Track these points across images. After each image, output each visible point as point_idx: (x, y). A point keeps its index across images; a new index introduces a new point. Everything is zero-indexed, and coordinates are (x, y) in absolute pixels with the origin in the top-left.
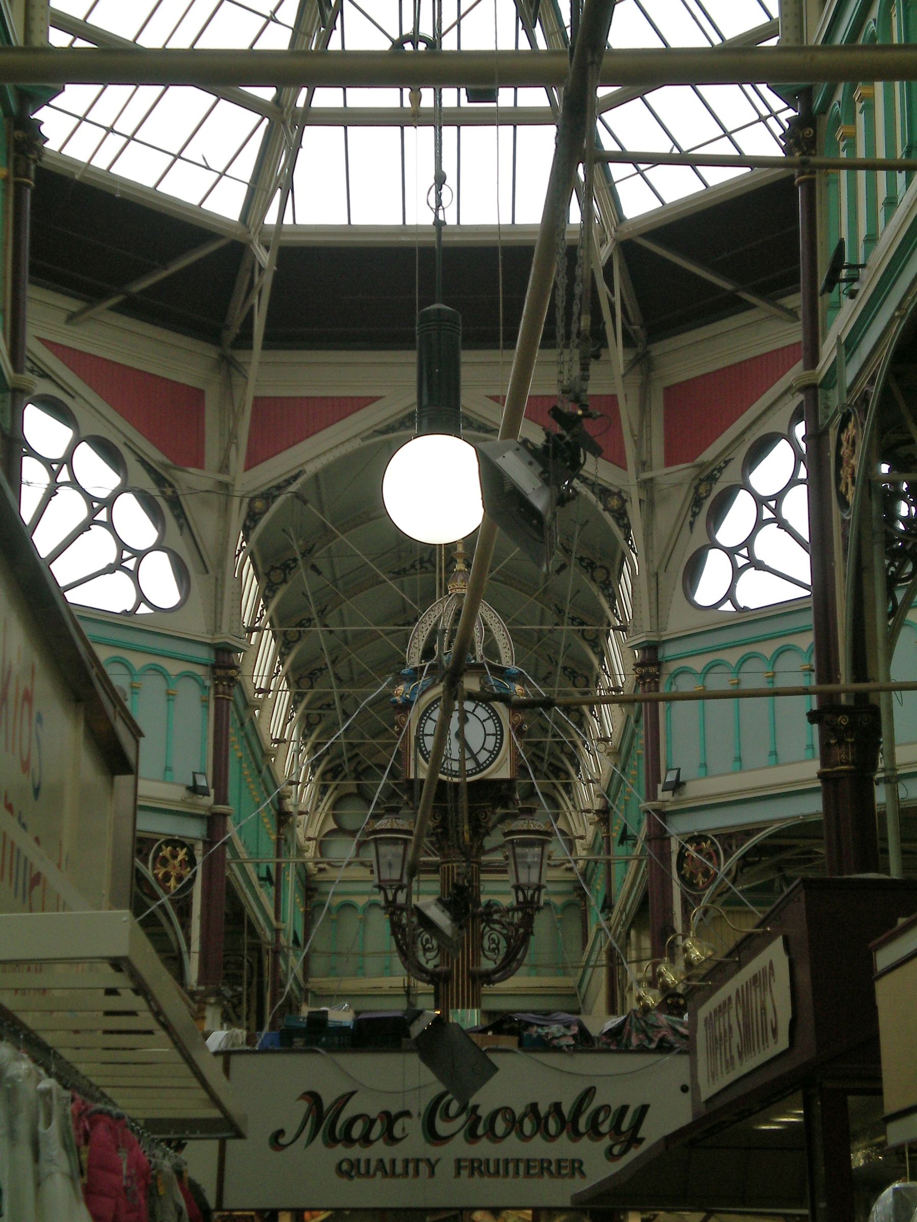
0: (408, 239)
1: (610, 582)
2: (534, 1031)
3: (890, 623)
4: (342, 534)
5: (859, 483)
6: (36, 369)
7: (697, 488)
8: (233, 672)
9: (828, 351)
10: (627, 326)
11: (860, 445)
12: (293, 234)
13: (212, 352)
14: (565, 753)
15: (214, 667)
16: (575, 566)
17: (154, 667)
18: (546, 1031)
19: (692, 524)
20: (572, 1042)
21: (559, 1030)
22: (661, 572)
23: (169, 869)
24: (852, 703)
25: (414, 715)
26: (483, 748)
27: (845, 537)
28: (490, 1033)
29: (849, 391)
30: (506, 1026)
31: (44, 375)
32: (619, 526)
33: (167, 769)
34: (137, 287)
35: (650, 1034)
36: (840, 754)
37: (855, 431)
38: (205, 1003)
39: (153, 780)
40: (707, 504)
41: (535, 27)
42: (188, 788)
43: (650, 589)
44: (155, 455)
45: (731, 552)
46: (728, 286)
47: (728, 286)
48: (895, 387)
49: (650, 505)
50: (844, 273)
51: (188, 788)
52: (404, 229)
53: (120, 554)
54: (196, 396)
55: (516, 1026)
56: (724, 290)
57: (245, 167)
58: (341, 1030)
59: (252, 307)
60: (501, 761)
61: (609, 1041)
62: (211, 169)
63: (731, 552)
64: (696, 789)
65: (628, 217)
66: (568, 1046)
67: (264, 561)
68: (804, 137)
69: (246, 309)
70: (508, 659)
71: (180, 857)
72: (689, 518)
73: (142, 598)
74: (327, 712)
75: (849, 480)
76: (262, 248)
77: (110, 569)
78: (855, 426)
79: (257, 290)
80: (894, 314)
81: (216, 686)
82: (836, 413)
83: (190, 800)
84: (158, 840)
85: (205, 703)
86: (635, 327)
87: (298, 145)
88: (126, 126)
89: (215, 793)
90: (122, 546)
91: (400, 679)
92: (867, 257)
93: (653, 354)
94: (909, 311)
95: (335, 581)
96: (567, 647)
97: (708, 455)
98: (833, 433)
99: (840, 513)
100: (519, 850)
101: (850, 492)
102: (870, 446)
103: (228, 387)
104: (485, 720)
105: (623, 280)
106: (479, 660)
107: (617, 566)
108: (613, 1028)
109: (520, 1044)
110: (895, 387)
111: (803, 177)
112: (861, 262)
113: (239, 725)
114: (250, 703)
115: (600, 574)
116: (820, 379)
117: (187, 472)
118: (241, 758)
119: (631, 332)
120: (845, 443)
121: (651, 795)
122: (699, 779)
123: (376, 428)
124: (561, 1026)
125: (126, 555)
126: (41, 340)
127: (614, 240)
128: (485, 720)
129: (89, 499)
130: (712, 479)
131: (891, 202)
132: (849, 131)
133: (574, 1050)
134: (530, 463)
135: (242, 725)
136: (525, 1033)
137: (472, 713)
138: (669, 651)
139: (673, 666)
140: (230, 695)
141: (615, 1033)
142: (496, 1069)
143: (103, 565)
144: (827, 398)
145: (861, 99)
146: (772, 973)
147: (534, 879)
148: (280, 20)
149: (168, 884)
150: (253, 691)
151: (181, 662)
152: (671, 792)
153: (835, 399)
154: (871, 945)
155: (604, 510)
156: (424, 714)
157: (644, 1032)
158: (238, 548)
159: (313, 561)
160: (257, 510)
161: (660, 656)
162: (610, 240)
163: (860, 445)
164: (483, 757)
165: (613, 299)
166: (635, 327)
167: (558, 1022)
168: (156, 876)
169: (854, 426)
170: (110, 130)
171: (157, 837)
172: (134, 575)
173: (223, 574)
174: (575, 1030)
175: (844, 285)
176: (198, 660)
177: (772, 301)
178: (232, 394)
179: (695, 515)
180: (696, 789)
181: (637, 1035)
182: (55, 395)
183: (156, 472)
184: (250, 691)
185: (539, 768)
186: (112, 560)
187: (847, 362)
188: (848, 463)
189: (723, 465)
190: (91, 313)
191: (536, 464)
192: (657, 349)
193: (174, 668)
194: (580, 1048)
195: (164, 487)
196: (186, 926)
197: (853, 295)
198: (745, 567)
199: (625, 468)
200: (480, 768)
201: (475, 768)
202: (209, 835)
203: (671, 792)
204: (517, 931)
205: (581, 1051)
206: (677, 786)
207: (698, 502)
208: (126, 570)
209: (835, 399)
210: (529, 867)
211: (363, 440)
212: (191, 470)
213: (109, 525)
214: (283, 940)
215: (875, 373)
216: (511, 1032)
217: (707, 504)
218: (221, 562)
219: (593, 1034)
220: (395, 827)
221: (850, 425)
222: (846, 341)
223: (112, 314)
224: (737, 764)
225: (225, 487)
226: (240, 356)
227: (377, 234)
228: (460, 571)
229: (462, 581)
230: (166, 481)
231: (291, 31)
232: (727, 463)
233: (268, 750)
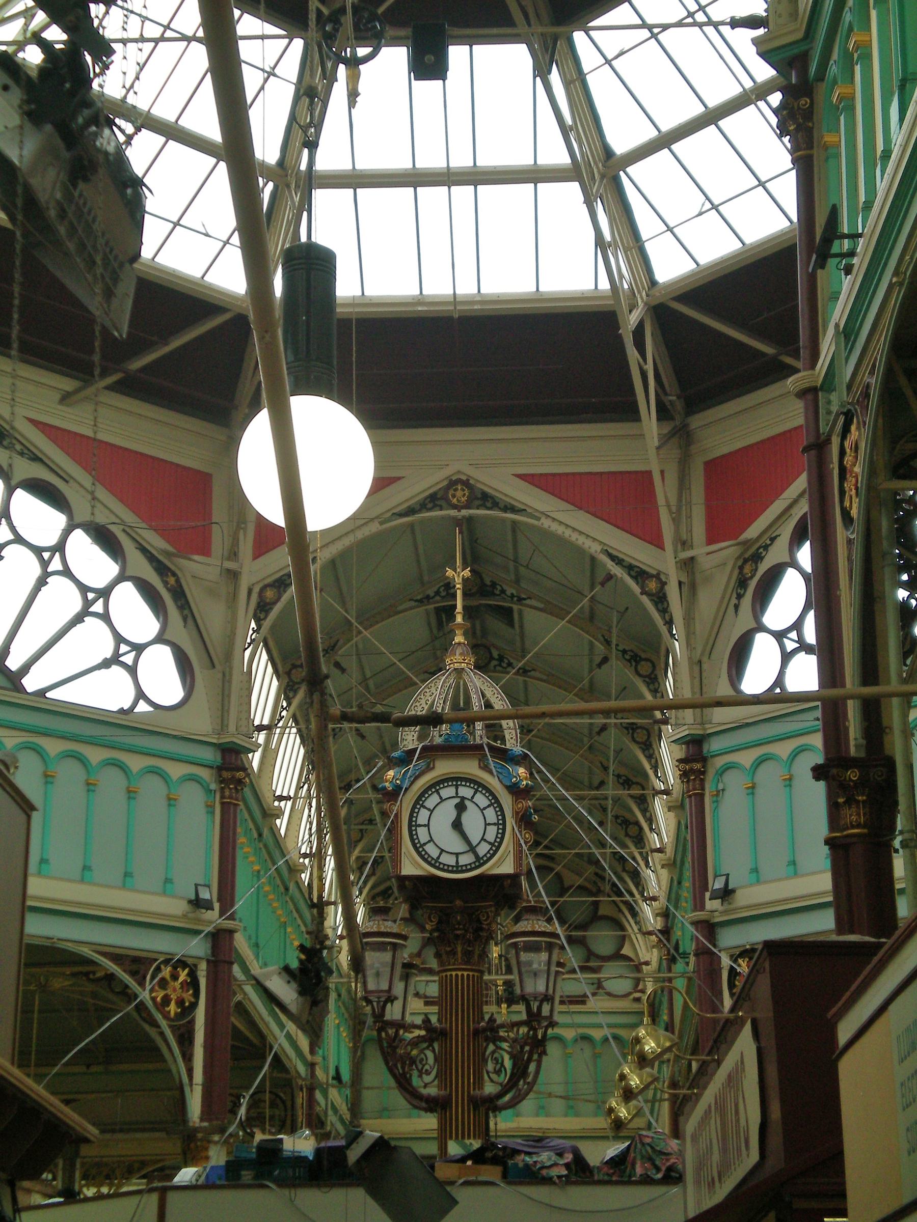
0: (425, 308)
1: (656, 675)
2: (522, 1160)
3: (908, 662)
4: (366, 629)
5: (863, 492)
6: (26, 451)
7: (741, 568)
8: (240, 774)
10: (663, 397)
14: (627, 872)
15: (220, 769)
16: (617, 658)
17: (152, 769)
18: (535, 1159)
19: (737, 607)
20: (565, 1172)
21: (550, 1159)
22: (705, 659)
23: (169, 992)
24: (862, 754)
25: (407, 802)
26: (483, 839)
27: (849, 559)
28: (469, 1163)
30: (489, 1155)
31: (35, 458)
32: (658, 610)
33: (167, 881)
34: (136, 364)
35: (658, 1163)
36: (851, 815)
38: (209, 1142)
39: (153, 894)
40: (753, 584)
41: (549, 72)
42: (190, 902)
43: (692, 678)
44: (156, 542)
45: (780, 636)
49: (690, 588)
51: (190, 902)
52: (420, 300)
53: (117, 648)
55: (501, 1153)
56: (764, 354)
58: (299, 1160)
60: (503, 855)
61: (612, 1171)
62: (210, 236)
63: (780, 636)
64: (747, 897)
66: (559, 1177)
67: (284, 659)
68: (799, 108)
69: (256, 383)
70: (513, 741)
71: (181, 979)
72: (734, 601)
73: (140, 695)
74: (369, 827)
75: (854, 492)
77: (106, 664)
78: (858, 428)
80: (891, 280)
81: (222, 789)
83: (190, 915)
84: (156, 960)
85: (210, 808)
86: (671, 398)
89: (220, 907)
90: (119, 639)
91: (393, 763)
92: (863, 227)
94: (908, 274)
95: (364, 681)
96: (618, 752)
97: (752, 532)
98: (835, 441)
99: (845, 531)
100: (524, 956)
101: (855, 506)
104: (485, 808)
106: (478, 741)
107: (663, 659)
108: (616, 1156)
109: (505, 1176)
111: (799, 153)
112: (860, 231)
113: (255, 835)
114: (268, 812)
115: (645, 668)
116: (820, 382)
117: (190, 559)
118: (259, 872)
119: (667, 404)
120: (848, 450)
121: (699, 905)
122: (751, 885)
123: (395, 511)
124: (552, 1154)
125: (124, 648)
126: (31, 421)
127: (646, 304)
128: (485, 808)
129: (84, 589)
130: (757, 558)
132: (847, 90)
133: (567, 1181)
135: (260, 835)
136: (510, 1162)
137: (471, 800)
138: (714, 746)
139: (720, 762)
140: (237, 800)
141: (619, 1162)
142: (454, 1202)
143: (99, 660)
144: (829, 402)
146: (743, 1070)
147: (541, 988)
148: (278, 74)
149: (167, 1009)
150: (272, 798)
151: (181, 764)
152: (720, 901)
153: (836, 401)
154: (830, 1015)
155: (642, 594)
156: (416, 802)
157: (650, 1159)
158: (249, 641)
159: (338, 659)
160: (268, 601)
161: (705, 751)
164: (483, 849)
165: (645, 367)
166: (671, 398)
167: (550, 1148)
168: (154, 999)
171: (154, 956)
172: (132, 670)
173: (231, 668)
174: (569, 1157)
176: (205, 762)
179: (739, 597)
180: (747, 897)
181: (642, 1164)
182: (46, 479)
183: (159, 561)
184: (267, 798)
185: (602, 889)
186: (108, 655)
188: (851, 472)
189: (768, 542)
192: (696, 421)
193: (176, 771)
194: (573, 1178)
195: (167, 575)
196: (188, 1057)
198: (795, 652)
199: (661, 547)
200: (480, 861)
201: (474, 863)
202: (213, 954)
203: (720, 901)
204: (522, 1048)
205: (575, 1183)
206: (726, 893)
207: (742, 583)
208: (124, 665)
209: (836, 401)
210: (535, 974)
211: (381, 523)
212: (196, 557)
213: (105, 617)
214: (319, 1073)
216: (495, 1161)
217: (753, 584)
218: (228, 656)
219: (592, 1164)
220: (383, 929)
221: (853, 428)
224: (791, 868)
225: (233, 576)
228: (459, 644)
229: (461, 654)
230: (169, 569)
231: (294, 86)
232: (773, 539)
233: (295, 866)
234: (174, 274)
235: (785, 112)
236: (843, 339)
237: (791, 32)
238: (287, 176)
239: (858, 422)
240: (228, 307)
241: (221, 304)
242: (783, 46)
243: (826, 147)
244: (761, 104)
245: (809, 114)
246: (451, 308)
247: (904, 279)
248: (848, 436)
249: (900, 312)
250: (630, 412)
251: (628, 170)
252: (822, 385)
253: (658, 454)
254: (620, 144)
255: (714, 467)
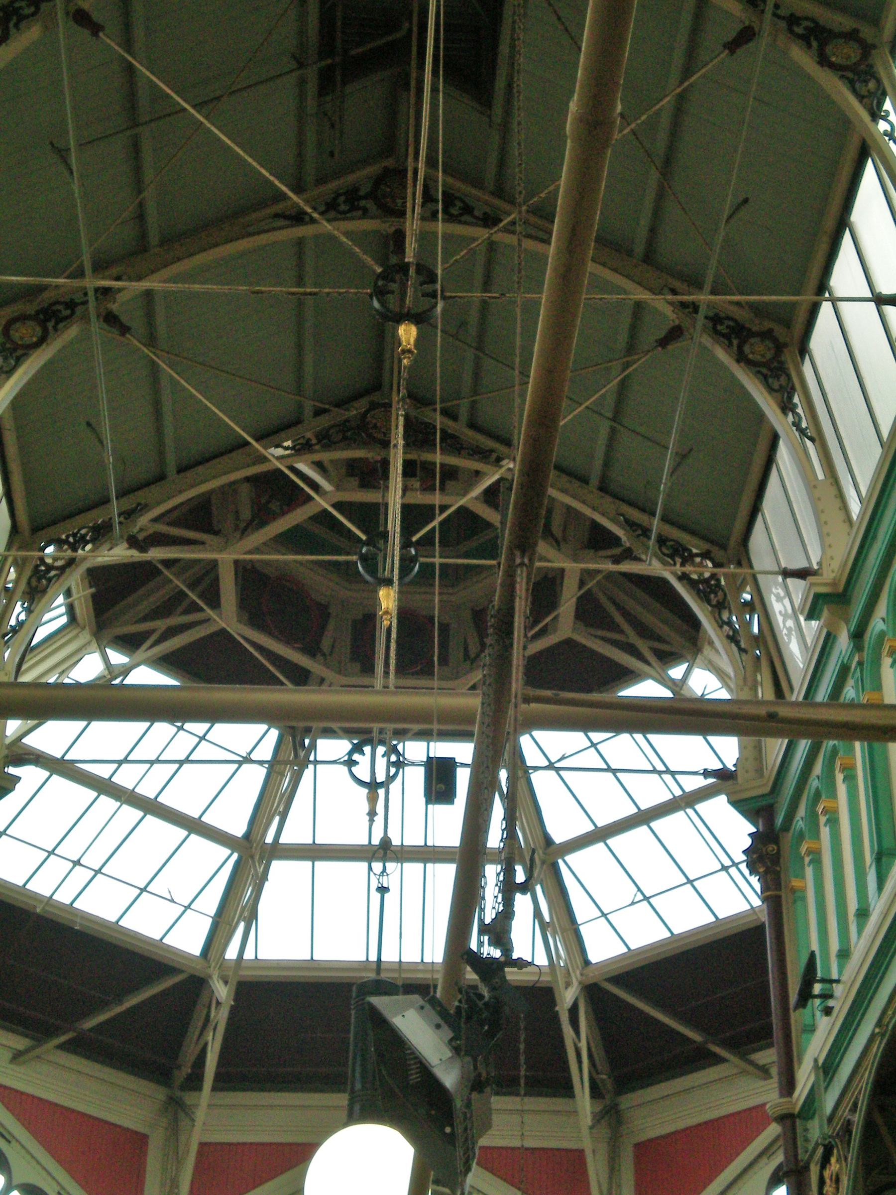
9: (805, 1077)
10: (594, 1074)
11: (845, 1181)
12: (254, 968)
13: (160, 1094)
29: (830, 1119)
37: (838, 1166)
46: (695, 1036)
47: (695, 1036)
48: (879, 1119)
50: (817, 988)
54: (140, 1140)
57: (211, 901)
59: (206, 1044)
62: (175, 903)
65: (594, 962)
69: (200, 1046)
76: (221, 982)
79: (214, 1024)
80: (873, 1031)
82: (817, 1145)
87: (264, 877)
88: (93, 860)
92: (840, 972)
93: (623, 1106)
102: (855, 1181)
103: (174, 1131)
105: (589, 1026)
110: (879, 1119)
119: (598, 1082)
120: (828, 1181)
127: (580, 983)
131: (863, 914)
134: (438, 1026)
144: (806, 1130)
145: (825, 811)
153: (815, 1130)
162: (575, 983)
163: (845, 1181)
165: (580, 1045)
169: (837, 1161)
170: (77, 863)
175: (818, 1001)
177: (743, 1056)
178: (177, 1141)
187: (826, 1088)
190: (38, 1051)
191: (445, 1027)
192: (628, 1101)
197: (828, 1011)
209: (815, 1130)
215: (857, 1099)
221: (833, 1160)
222: (824, 1064)
223: (60, 1052)
226: (189, 1098)
227: (337, 969)
234: (136, 936)
235: (755, 856)
236: (822, 1074)
237: (759, 787)
238: (251, 848)
239: (839, 1155)
240: (184, 968)
241: (174, 964)
242: (752, 798)
243: (793, 891)
244: (690, 811)
245: (776, 859)
246: (396, 975)
247: (886, 1032)
248: (828, 1166)
249: (882, 1057)
250: (565, 1089)
251: (567, 858)
252: (799, 1113)
253: (591, 1133)
254: (559, 834)
255: (642, 1148)
